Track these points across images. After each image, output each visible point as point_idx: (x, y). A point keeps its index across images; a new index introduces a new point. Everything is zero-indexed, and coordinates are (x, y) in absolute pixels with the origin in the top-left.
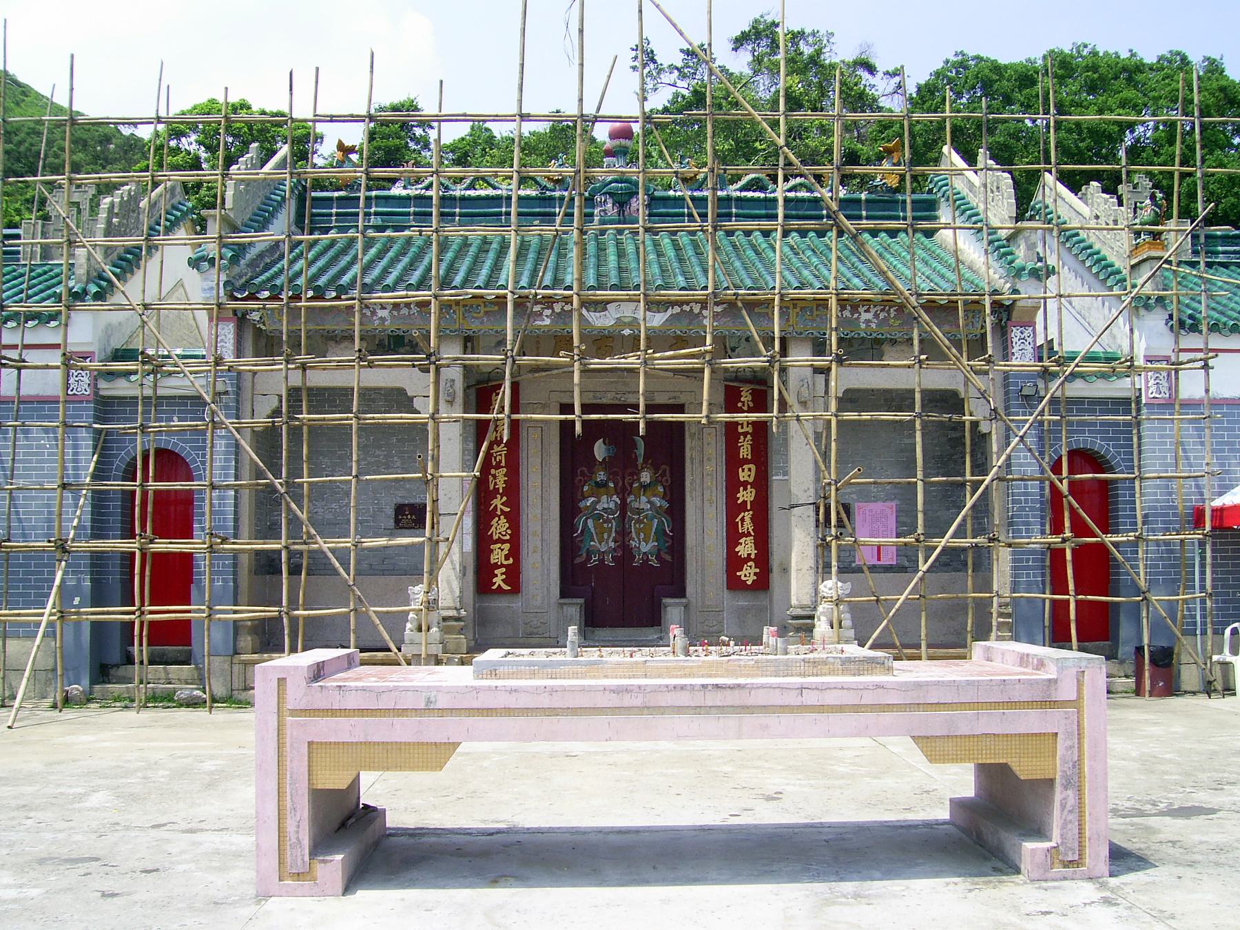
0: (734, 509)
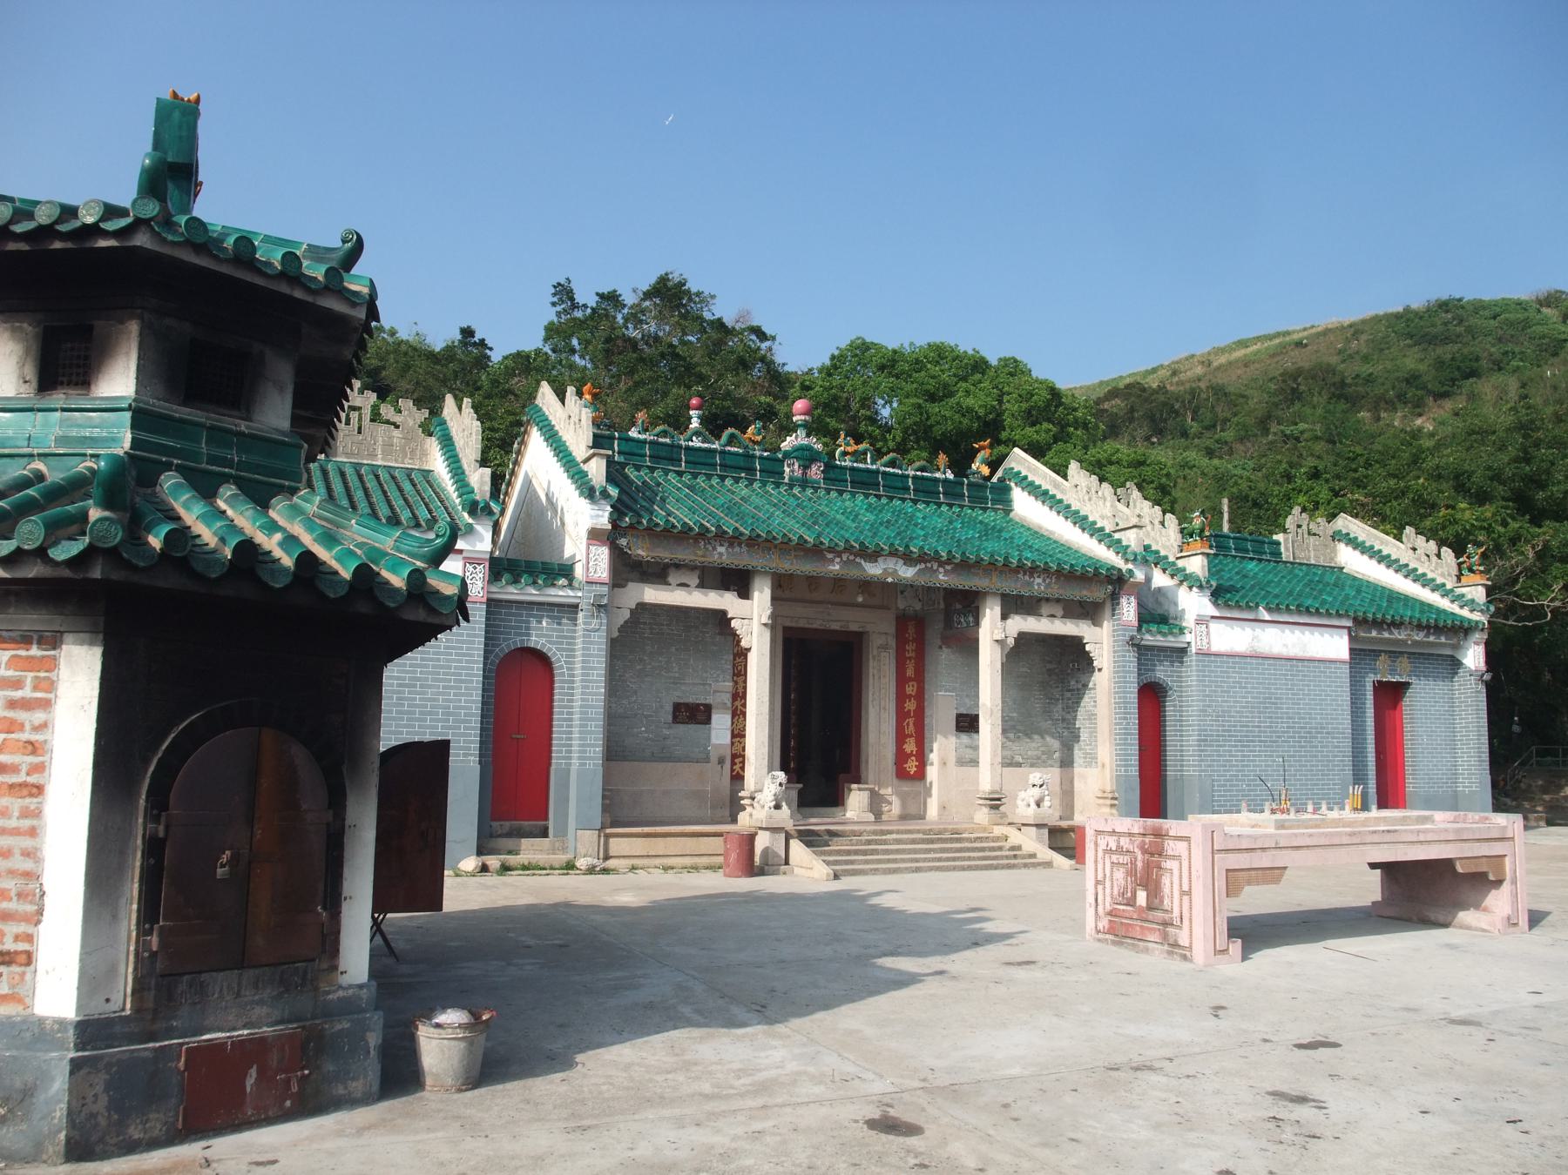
0: (901, 715)
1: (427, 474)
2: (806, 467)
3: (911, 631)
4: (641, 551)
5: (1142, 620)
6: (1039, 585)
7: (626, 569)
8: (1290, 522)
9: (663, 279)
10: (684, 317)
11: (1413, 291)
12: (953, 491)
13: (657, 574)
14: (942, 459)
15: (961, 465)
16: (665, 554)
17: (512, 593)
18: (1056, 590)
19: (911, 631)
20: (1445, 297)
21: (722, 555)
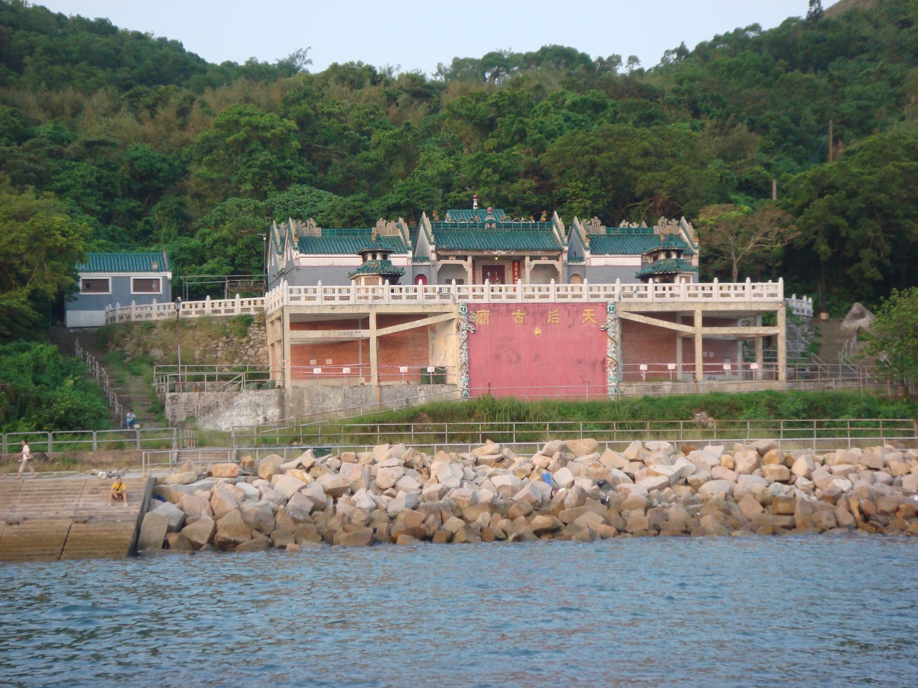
1: (399, 237)
2: (491, 225)
3: (516, 264)
4: (442, 253)
5: (569, 259)
6: (539, 253)
7: (439, 258)
8: (660, 222)
9: (252, 59)
10: (471, 118)
11: (726, 27)
12: (534, 226)
13: (447, 257)
14: (532, 217)
15: (537, 218)
16: (447, 254)
17: (416, 264)
18: (543, 253)
19: (516, 264)
20: (232, 61)
21: (459, 253)
